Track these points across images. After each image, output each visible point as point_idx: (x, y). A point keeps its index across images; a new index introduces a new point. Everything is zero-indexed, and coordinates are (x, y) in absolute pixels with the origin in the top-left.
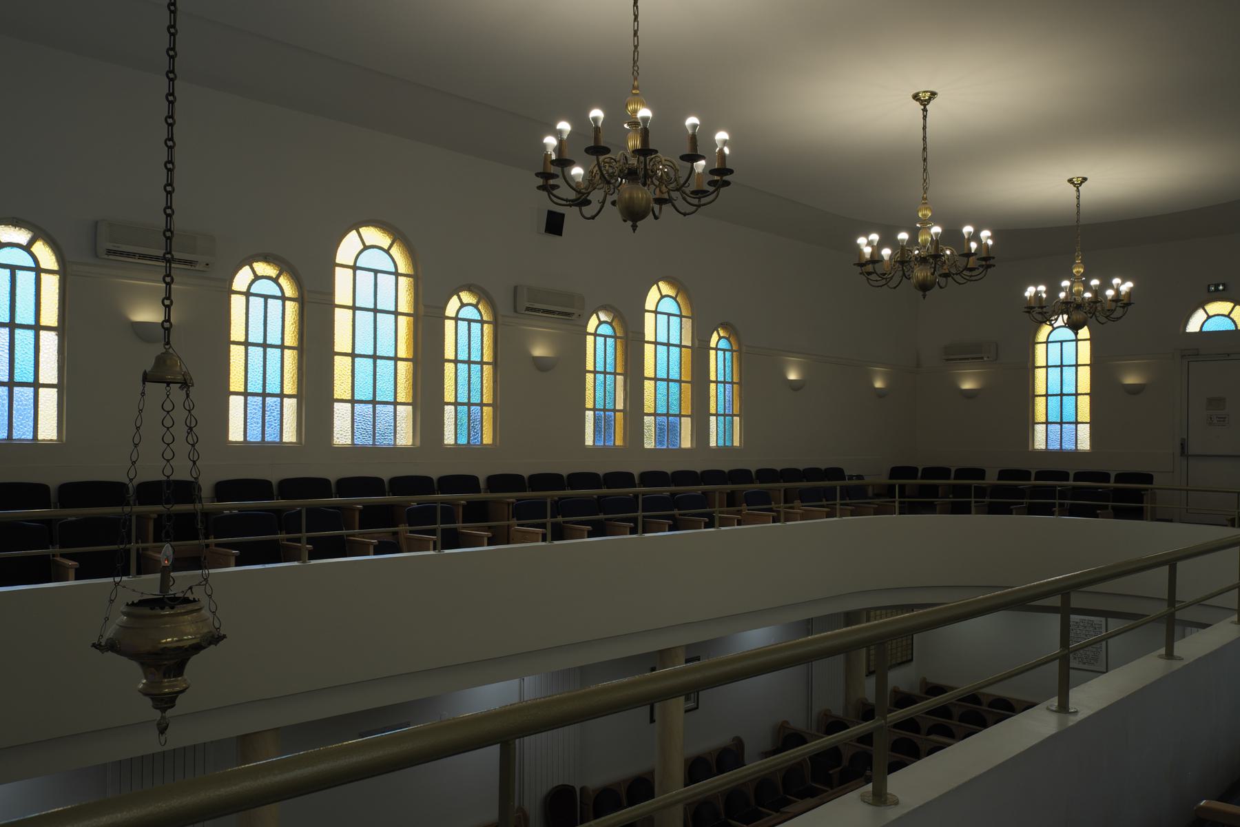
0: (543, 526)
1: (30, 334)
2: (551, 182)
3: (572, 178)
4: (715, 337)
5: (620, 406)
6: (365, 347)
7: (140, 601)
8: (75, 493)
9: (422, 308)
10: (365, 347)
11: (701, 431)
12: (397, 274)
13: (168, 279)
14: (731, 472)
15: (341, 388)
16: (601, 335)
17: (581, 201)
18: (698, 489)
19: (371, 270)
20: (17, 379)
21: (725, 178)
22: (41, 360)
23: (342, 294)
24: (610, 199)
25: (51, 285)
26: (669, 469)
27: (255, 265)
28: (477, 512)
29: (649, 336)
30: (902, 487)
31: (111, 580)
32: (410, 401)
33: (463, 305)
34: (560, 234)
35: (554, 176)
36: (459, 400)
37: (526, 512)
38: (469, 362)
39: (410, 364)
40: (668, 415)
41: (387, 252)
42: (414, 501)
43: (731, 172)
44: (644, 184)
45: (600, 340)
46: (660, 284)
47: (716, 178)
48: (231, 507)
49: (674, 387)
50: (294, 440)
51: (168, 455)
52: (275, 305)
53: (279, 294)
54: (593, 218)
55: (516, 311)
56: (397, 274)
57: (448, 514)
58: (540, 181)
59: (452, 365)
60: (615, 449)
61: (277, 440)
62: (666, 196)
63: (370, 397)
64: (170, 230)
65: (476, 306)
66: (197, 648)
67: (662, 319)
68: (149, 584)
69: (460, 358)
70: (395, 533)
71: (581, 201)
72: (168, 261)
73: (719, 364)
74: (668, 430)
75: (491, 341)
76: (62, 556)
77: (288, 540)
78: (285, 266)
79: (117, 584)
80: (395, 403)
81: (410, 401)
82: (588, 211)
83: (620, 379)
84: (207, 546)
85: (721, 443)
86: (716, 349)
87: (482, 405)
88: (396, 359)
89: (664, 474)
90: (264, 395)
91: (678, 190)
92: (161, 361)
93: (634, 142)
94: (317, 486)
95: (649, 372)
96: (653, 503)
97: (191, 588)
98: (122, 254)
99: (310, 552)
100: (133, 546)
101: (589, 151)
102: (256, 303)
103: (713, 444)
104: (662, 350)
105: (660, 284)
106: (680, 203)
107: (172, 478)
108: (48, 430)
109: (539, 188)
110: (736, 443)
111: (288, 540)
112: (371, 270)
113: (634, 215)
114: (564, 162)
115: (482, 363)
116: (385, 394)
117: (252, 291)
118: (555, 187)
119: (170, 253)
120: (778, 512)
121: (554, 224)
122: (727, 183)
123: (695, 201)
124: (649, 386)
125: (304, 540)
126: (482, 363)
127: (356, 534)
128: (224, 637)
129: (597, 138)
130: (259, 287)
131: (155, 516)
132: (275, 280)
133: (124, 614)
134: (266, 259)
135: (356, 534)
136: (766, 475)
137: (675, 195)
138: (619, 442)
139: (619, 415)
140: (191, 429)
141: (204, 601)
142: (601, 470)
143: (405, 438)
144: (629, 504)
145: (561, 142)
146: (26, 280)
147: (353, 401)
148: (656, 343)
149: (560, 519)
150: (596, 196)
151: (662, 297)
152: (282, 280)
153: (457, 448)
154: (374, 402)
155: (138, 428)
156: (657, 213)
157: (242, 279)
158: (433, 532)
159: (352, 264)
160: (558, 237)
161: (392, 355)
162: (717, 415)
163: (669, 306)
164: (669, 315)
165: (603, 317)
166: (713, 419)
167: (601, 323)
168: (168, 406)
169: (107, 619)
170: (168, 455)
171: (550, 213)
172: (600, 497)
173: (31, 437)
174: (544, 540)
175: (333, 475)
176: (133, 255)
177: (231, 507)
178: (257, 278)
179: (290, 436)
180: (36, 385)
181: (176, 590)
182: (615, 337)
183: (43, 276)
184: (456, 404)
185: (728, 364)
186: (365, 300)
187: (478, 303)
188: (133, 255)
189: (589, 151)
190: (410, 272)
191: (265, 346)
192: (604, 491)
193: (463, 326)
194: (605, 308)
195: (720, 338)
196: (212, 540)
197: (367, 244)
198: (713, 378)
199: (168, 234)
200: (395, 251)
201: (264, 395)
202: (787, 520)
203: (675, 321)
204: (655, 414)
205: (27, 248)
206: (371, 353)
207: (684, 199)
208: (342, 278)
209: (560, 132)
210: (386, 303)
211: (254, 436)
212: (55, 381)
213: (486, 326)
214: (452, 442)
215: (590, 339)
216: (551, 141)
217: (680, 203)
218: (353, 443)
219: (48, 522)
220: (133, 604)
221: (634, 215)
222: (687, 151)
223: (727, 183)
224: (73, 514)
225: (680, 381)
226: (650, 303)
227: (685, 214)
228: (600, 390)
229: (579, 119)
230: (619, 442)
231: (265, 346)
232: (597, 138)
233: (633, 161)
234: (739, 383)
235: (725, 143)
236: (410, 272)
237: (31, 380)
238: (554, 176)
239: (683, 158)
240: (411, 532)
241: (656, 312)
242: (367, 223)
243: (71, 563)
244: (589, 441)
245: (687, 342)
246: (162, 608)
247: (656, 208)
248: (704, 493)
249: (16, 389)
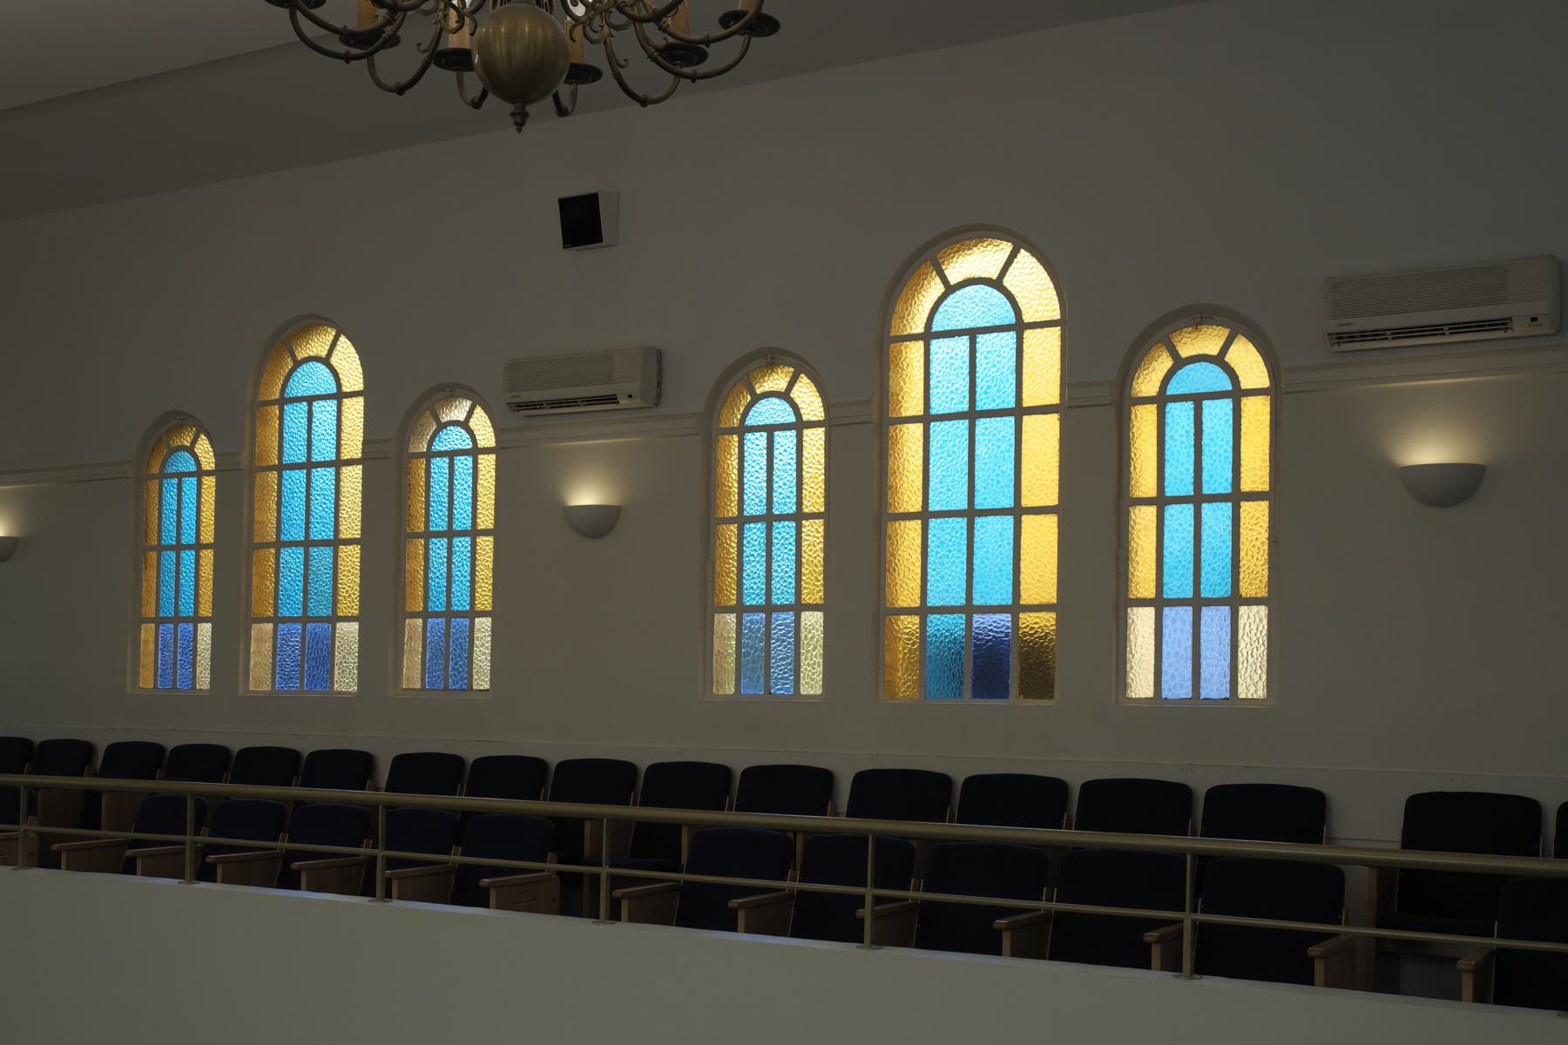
25: (1257, 413)
41: (950, 289)
52: (1217, 414)
53: (1227, 385)
96: (409, 829)
98: (1364, 336)
102: (1179, 415)
126: (474, 533)
134: (1199, 317)
144: (357, 824)
176: (1377, 334)
178: (1179, 363)
179: (1253, 685)
188: (1377, 334)
197: (1007, 282)
211: (1178, 687)
227: (644, 102)
228: (778, 560)
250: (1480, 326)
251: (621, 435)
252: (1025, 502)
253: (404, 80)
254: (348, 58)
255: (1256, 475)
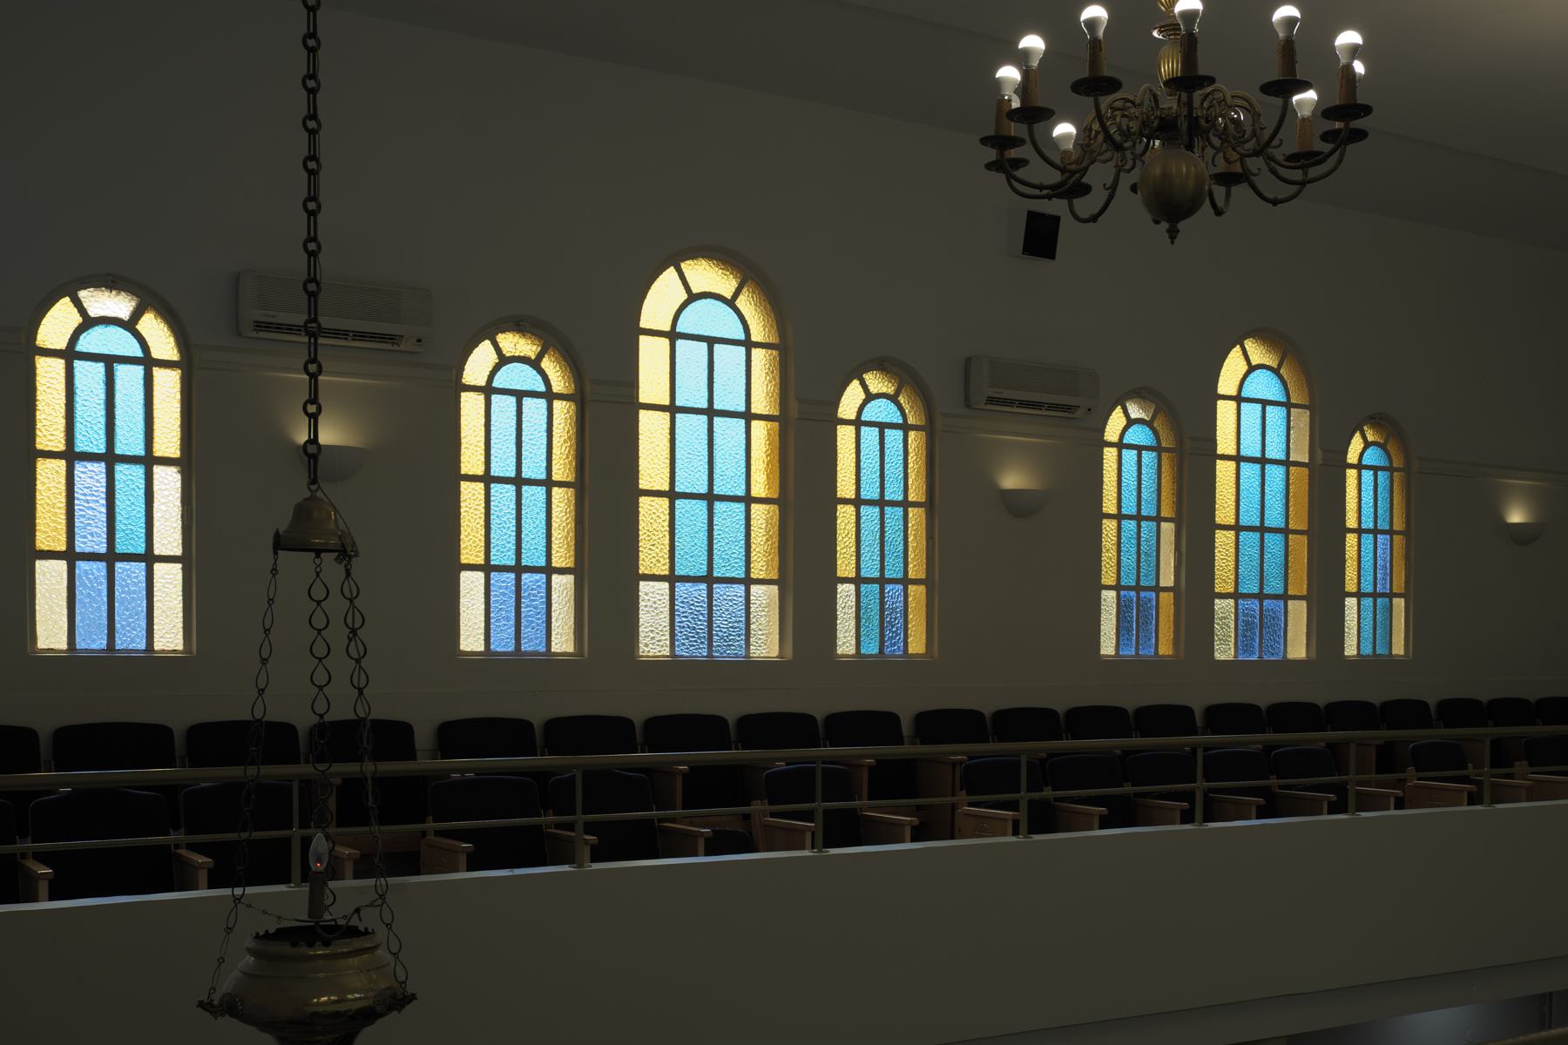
0: (1012, 806)
1: (138, 471)
2: (1013, 153)
3: (1054, 143)
4: (1356, 444)
5: (1167, 580)
6: (692, 478)
7: (279, 931)
8: (214, 741)
9: (1319, 453)
10: (692, 478)
11: (1326, 625)
12: (748, 344)
13: (313, 368)
14: (1493, 703)
15: (652, 556)
16: (1368, 467)
17: (1072, 188)
18: (1317, 739)
19: (700, 335)
20: (120, 548)
21: (1357, 124)
22: (157, 515)
23: (652, 386)
24: (1126, 180)
25: (168, 384)
26: (1376, 696)
27: (501, 338)
28: (896, 780)
29: (1225, 444)
30: (1497, 744)
31: (227, 892)
32: (774, 575)
33: (870, 397)
34: (1052, 256)
35: (1016, 142)
36: (864, 574)
37: (987, 780)
38: (881, 503)
39: (774, 508)
40: (1261, 596)
41: (731, 303)
42: (779, 759)
43: (1366, 110)
44: (1190, 147)
45: (1130, 456)
46: (1248, 344)
47: (1338, 125)
48: (463, 766)
49: (1274, 542)
50: (571, 649)
51: (321, 678)
52: (535, 409)
53: (542, 388)
54: (1094, 219)
55: (968, 405)
56: (748, 344)
57: (839, 781)
58: (991, 154)
59: (850, 509)
60: (1158, 663)
61: (542, 649)
62: (1238, 169)
63: (703, 571)
64: (314, 280)
65: (893, 398)
66: (368, 1016)
67: (1251, 412)
68: (282, 900)
69: (865, 495)
70: (746, 817)
71: (1072, 188)
72: (311, 335)
73: (1361, 496)
74: (1261, 621)
75: (922, 463)
76: (190, 847)
77: (558, 826)
78: (552, 338)
79: (237, 900)
80: (748, 581)
81: (774, 575)
82: (1085, 205)
83: (1168, 528)
84: (424, 834)
85: (1367, 650)
86: (1359, 467)
87: (905, 581)
88: (748, 500)
89: (1252, 708)
90: (519, 569)
91: (1256, 153)
92: (303, 512)
93: (1169, 67)
94: (606, 732)
95: (1224, 514)
96: (1221, 765)
97: (357, 911)
99: (1102, 817)
100: (296, 833)
101: (1080, 87)
103: (1350, 650)
104: (1250, 471)
105: (1248, 344)
106: (1266, 182)
107: (327, 718)
108: (170, 636)
109: (989, 166)
110: (1399, 649)
111: (558, 826)
112: (700, 335)
113: (1171, 209)
114: (1035, 114)
115: (905, 504)
116: (729, 563)
117: (496, 384)
118: (1020, 163)
119: (315, 320)
120: (1479, 783)
121: (1040, 238)
122: (1360, 135)
123: (1297, 175)
124: (1224, 540)
125: (580, 827)
126: (905, 504)
127: (677, 817)
128: (413, 997)
129: (1094, 61)
130: (92, 341)
131: (338, 781)
132: (535, 364)
133: (251, 951)
134: (112, 282)
135: (677, 817)
136: (1458, 711)
137: (1255, 164)
138: (1165, 649)
139: (1167, 599)
140: (354, 631)
141: (381, 934)
142: (1130, 703)
143: (766, 644)
144: (1180, 766)
145: (1026, 74)
146: (129, 378)
147: (672, 579)
148: (1238, 459)
149: (1048, 793)
150: (1098, 176)
151: (1252, 369)
152: (547, 364)
153: (860, 661)
154: (709, 579)
155: (267, 631)
156: (1220, 203)
157: (57, 325)
158: (808, 816)
159: (667, 327)
160: (1046, 262)
161: (741, 492)
162: (1359, 595)
163: (1265, 385)
164: (1264, 403)
165: (1135, 411)
166: (1351, 603)
167: (1131, 422)
168: (318, 593)
169: (221, 960)
170: (321, 678)
171: (1033, 217)
172: (1127, 753)
173: (142, 646)
174: (1016, 833)
175: (638, 711)
177: (463, 766)
178: (503, 360)
180: (149, 558)
181: (336, 913)
182: (1157, 449)
183: (77, 364)
184: (858, 581)
185: (1383, 494)
186: (692, 393)
187: (897, 393)
189: (1080, 87)
190: (773, 339)
191: (519, 481)
192: (1136, 741)
193: (870, 435)
194: (1140, 394)
195: (1367, 445)
196: (431, 825)
197: (695, 290)
198: (1351, 522)
199: (312, 287)
200: (745, 303)
201: (519, 569)
202: (1496, 800)
203: (1276, 415)
204: (1236, 596)
205: (130, 325)
206: (703, 490)
207: (1273, 172)
208: (652, 353)
209: (1026, 53)
210: (729, 397)
211: (503, 642)
212: (178, 551)
213: (912, 434)
214: (479, 646)
215: (1110, 454)
216: (1009, 73)
217: (1266, 182)
218: (710, 655)
219: (169, 790)
220: (267, 936)
221: (1171, 209)
222: (1274, 74)
223: (1360, 135)
224: (208, 776)
225: (1285, 531)
226: (1227, 382)
227: (1275, 202)
229: (1061, 25)
230: (1165, 649)
231: (519, 481)
232: (1094, 61)
233: (1170, 103)
234: (1405, 533)
235: (1354, 51)
236: (773, 339)
237: (141, 550)
238: (1016, 142)
239: (1268, 89)
240: (773, 815)
241: (1239, 399)
242: (694, 254)
243: (201, 859)
244: (1108, 648)
245: (1301, 454)
246: (311, 945)
247: (1219, 192)
248: (1332, 746)
249: (119, 565)
250: (373, 337)
251: (1034, 436)
252: (717, 491)
253: (1096, 211)
254: (1340, 161)
255: (168, 442)
